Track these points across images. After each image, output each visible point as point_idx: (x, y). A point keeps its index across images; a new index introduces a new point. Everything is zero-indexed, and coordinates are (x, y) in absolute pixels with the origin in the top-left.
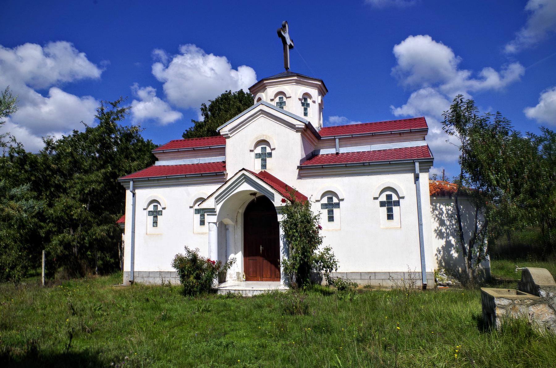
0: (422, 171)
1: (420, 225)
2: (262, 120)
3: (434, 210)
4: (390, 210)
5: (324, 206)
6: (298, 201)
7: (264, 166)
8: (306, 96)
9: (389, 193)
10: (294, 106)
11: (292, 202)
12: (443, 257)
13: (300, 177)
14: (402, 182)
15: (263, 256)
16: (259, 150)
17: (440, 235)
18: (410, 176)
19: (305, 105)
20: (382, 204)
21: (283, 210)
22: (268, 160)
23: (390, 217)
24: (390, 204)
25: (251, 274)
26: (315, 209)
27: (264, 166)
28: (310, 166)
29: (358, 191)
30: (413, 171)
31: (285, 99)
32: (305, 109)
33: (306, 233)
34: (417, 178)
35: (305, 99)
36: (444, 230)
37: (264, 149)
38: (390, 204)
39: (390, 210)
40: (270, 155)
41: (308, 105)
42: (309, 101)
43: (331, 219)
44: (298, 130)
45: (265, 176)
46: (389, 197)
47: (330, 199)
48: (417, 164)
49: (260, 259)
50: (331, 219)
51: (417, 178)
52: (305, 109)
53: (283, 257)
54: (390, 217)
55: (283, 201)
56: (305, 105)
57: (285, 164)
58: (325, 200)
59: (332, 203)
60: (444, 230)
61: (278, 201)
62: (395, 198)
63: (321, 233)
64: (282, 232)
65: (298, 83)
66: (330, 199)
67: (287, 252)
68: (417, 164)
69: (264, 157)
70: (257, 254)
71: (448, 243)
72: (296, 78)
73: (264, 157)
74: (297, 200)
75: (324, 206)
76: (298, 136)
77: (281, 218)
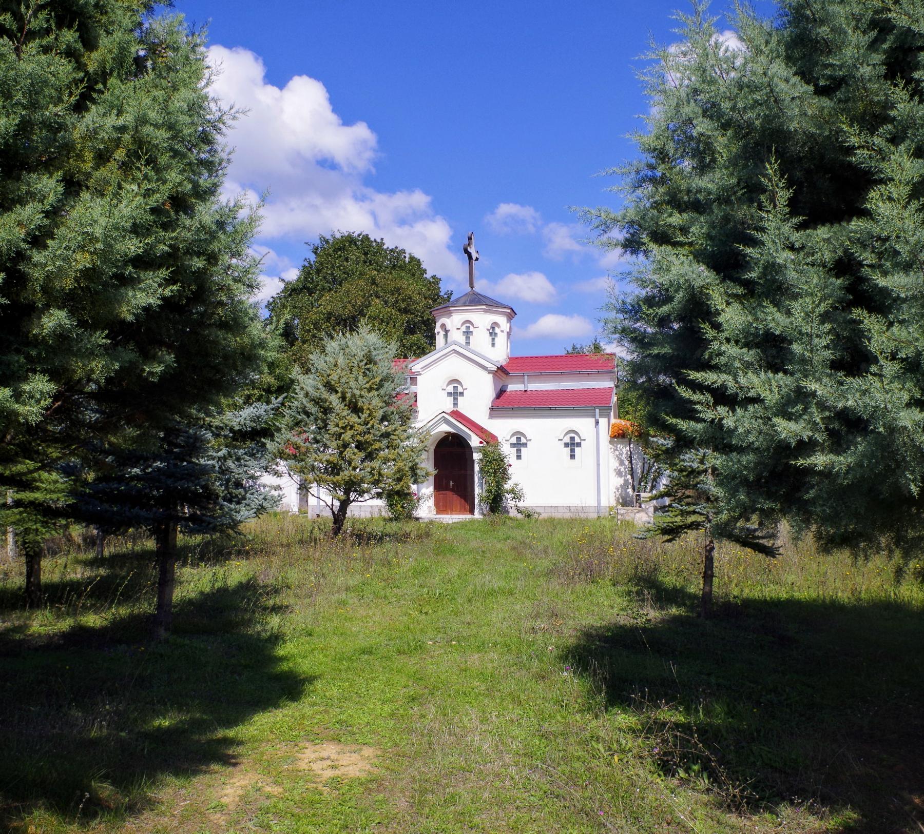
0: (601, 416)
1: (598, 465)
2: (454, 358)
3: (615, 450)
4: (572, 451)
5: (513, 445)
6: (492, 443)
7: (455, 405)
8: (494, 325)
9: (572, 435)
10: (480, 339)
11: (487, 443)
12: (621, 495)
13: (491, 416)
14: (583, 425)
15: (452, 490)
16: (450, 389)
17: (619, 474)
18: (591, 421)
19: (493, 334)
20: (566, 445)
21: (479, 450)
22: (460, 398)
23: (572, 457)
24: (572, 445)
25: (441, 507)
26: (506, 449)
27: (455, 405)
28: (503, 404)
29: (545, 432)
30: (594, 416)
31: (472, 329)
32: (493, 339)
33: (497, 468)
34: (597, 423)
35: (493, 328)
36: (622, 469)
37: (455, 388)
38: (572, 445)
39: (572, 451)
40: (462, 394)
41: (496, 334)
42: (497, 330)
43: (519, 457)
44: (490, 372)
45: (456, 414)
46: (572, 439)
47: (519, 439)
48: (597, 411)
49: (449, 494)
50: (519, 457)
51: (597, 423)
52: (493, 339)
53: (477, 490)
54: (572, 457)
55: (481, 443)
56: (493, 334)
57: (477, 402)
58: (514, 440)
59: (519, 444)
60: (622, 469)
61: (475, 441)
62: (577, 440)
63: (510, 471)
64: (477, 468)
65: (486, 311)
66: (519, 439)
67: (481, 485)
68: (597, 411)
69: (455, 395)
70: (447, 488)
71: (626, 481)
72: (484, 307)
73: (455, 395)
74: (489, 439)
75: (513, 445)
76: (490, 377)
77: (477, 456)
